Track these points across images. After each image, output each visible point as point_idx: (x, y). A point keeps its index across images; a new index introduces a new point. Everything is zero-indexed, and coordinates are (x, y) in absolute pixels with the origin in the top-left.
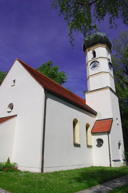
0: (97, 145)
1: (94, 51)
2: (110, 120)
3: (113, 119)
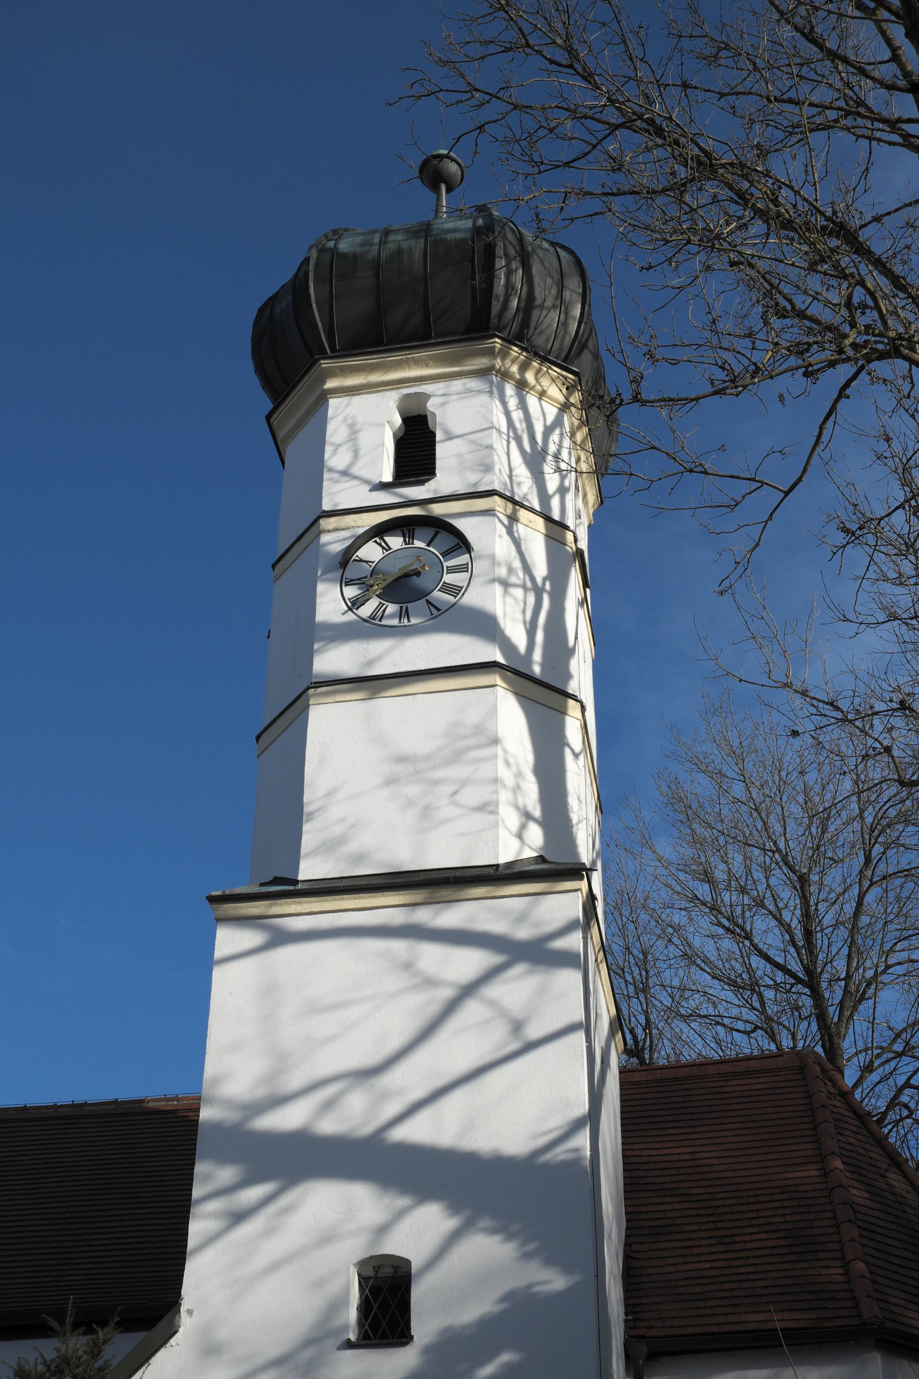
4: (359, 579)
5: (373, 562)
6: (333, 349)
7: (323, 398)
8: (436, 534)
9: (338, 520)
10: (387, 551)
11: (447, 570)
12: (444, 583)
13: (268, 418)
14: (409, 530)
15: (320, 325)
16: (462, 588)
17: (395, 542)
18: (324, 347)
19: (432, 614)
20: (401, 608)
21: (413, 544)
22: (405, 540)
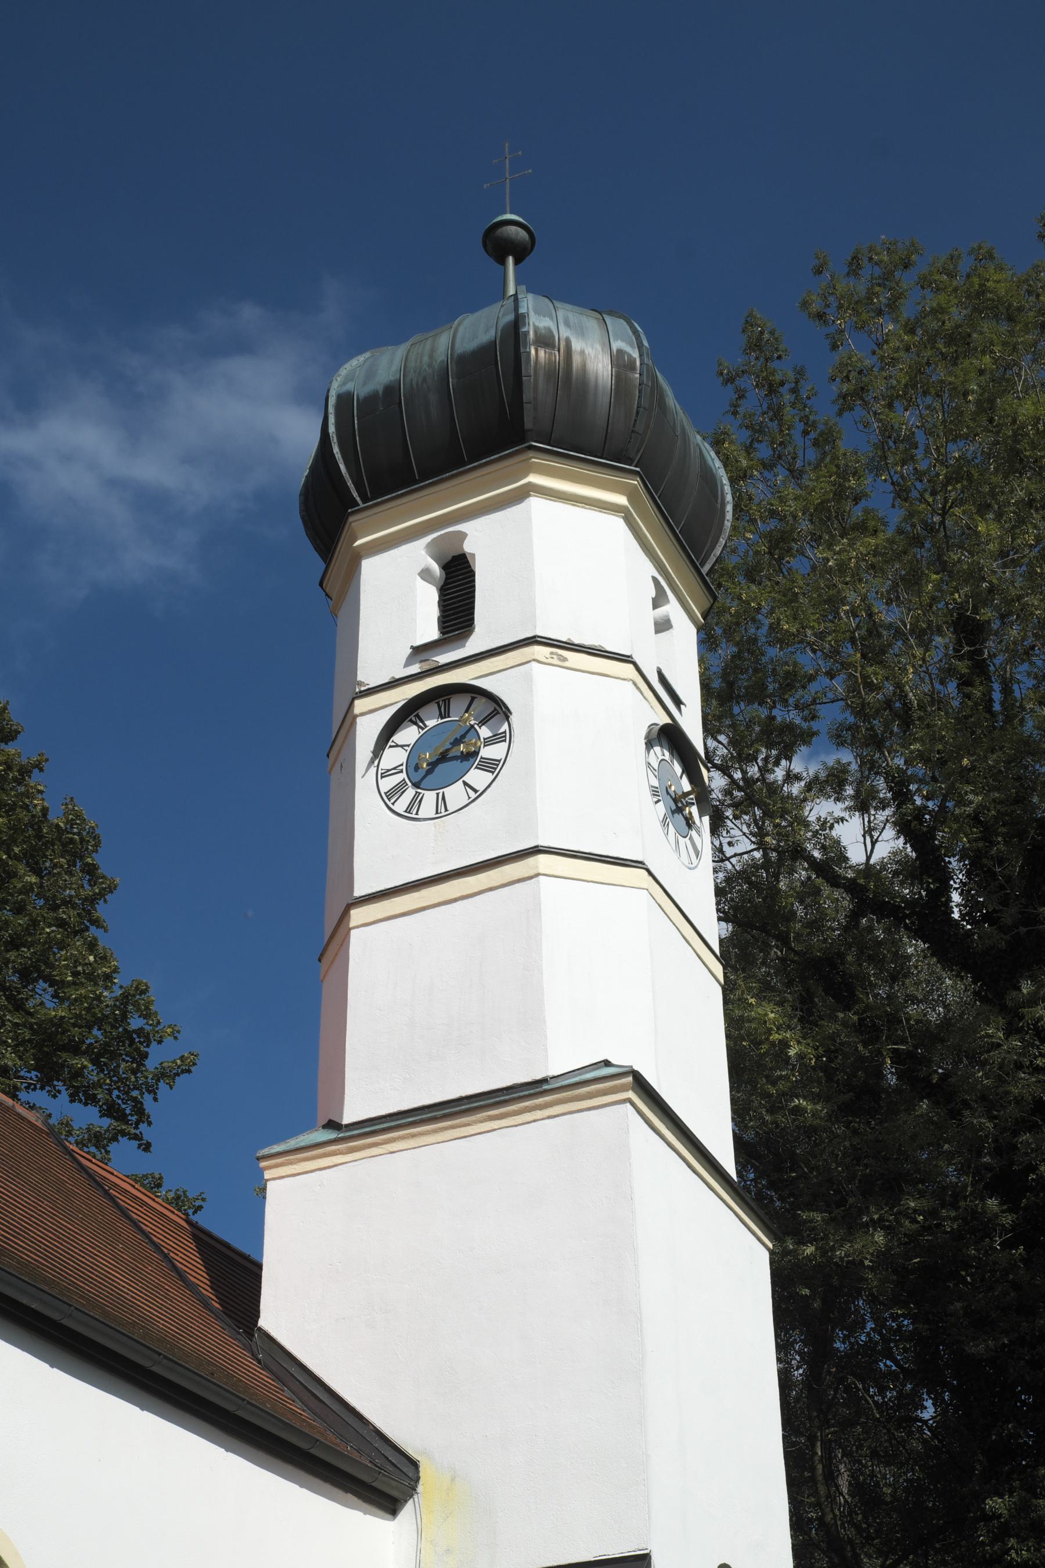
4: (394, 768)
5: (408, 746)
6: (365, 500)
10: (423, 729)
11: (405, 782)
12: (482, 758)
13: (321, 584)
14: (444, 701)
16: (499, 761)
17: (409, 735)
19: (469, 798)
20: (438, 794)
21: (426, 726)
22: (419, 727)
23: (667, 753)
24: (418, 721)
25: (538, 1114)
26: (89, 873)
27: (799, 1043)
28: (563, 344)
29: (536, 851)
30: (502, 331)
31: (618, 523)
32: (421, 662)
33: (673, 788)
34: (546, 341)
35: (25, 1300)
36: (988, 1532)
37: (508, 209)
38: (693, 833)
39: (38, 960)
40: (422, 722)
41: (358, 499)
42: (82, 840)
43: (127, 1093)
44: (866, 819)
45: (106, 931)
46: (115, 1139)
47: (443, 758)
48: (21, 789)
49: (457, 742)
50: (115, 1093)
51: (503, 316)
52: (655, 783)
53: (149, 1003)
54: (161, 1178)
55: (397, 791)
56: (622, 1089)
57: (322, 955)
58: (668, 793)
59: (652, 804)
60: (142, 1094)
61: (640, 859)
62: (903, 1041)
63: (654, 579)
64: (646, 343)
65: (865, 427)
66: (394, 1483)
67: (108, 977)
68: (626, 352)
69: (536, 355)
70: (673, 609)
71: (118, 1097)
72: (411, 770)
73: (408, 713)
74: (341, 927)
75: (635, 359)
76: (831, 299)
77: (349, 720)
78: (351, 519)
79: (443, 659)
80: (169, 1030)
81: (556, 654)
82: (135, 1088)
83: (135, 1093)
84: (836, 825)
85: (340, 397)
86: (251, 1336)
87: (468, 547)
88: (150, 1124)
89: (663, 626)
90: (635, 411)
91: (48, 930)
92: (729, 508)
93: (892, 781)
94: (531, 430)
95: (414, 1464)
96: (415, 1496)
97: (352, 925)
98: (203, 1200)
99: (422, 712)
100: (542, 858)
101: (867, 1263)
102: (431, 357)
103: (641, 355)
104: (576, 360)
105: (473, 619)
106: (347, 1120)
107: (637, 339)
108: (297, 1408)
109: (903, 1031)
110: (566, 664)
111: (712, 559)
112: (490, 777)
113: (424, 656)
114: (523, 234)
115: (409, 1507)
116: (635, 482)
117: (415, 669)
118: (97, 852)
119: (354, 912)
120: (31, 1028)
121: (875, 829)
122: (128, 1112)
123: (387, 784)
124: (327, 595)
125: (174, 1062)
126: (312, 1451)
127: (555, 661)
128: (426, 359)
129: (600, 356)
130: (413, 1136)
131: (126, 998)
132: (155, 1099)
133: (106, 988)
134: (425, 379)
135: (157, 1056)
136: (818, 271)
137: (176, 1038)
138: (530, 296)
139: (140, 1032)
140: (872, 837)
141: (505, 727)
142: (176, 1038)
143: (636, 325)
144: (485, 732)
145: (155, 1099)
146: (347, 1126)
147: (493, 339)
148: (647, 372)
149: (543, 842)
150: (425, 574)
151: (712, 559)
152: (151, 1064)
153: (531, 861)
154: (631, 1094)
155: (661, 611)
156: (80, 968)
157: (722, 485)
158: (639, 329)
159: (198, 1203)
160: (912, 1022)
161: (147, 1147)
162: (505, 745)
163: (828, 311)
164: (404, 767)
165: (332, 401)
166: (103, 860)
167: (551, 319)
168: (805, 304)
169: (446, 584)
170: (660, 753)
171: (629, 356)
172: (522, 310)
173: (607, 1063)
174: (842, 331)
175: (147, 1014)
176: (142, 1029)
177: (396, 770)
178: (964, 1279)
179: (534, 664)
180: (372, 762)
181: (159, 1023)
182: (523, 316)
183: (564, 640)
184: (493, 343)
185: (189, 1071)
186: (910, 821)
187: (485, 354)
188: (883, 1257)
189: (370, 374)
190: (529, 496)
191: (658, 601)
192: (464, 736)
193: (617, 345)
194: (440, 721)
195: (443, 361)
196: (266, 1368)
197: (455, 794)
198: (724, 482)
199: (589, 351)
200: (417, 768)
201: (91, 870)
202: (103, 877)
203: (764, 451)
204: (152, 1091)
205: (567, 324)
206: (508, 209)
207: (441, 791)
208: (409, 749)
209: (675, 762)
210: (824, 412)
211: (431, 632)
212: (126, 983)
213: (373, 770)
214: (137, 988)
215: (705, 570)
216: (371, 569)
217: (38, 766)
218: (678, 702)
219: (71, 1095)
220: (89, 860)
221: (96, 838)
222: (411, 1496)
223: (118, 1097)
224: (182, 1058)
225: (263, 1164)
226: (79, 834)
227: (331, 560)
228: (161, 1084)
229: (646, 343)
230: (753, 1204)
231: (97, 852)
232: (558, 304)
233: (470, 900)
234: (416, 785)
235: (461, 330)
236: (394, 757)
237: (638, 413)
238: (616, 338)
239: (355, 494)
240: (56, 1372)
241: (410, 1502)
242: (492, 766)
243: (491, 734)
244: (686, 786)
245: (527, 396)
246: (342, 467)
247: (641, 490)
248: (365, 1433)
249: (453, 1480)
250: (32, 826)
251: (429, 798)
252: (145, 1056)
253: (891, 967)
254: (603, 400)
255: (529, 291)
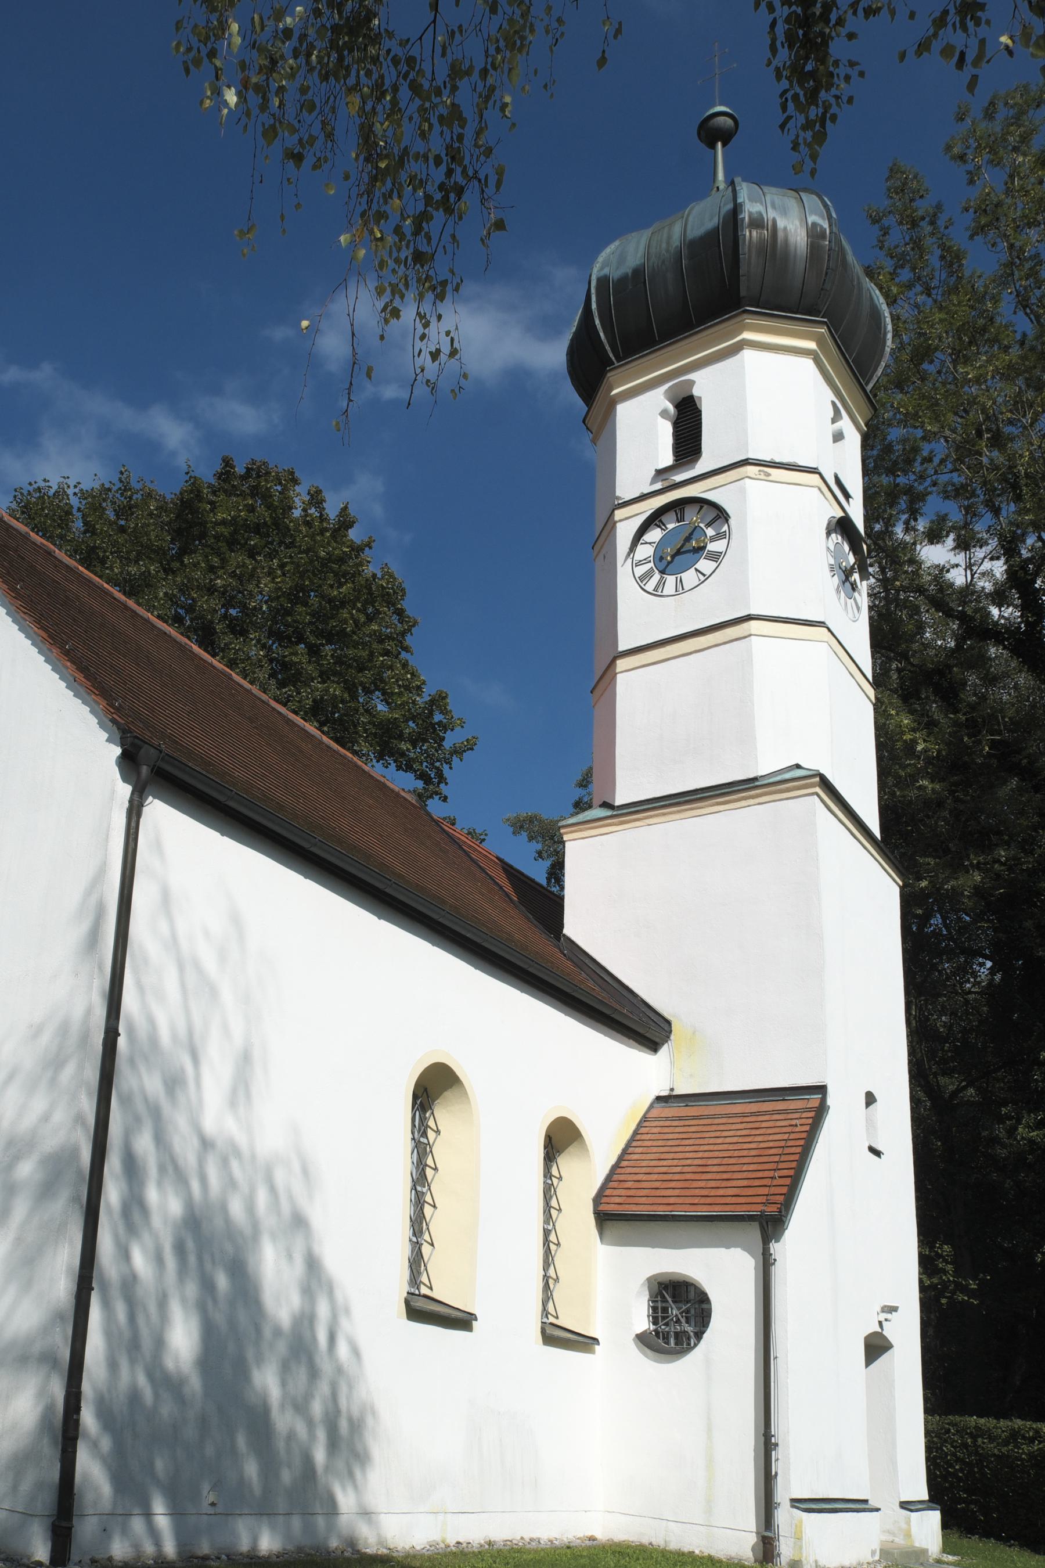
0: (642, 1339)
1: (653, 1045)
2: (794, 1103)
3: (830, 1101)
6: (619, 359)
7: (611, 405)
8: (701, 507)
9: (79, 1172)
13: (584, 422)
15: (717, 84)
17: (655, 535)
18: (611, 359)
22: (662, 529)
23: (839, 537)
24: (661, 525)
25: (751, 802)
26: (398, 615)
27: (925, 741)
28: (770, 223)
29: (749, 618)
30: (724, 217)
31: (809, 363)
32: (662, 480)
33: (844, 564)
34: (757, 223)
35: (463, 932)
36: (1041, 1073)
37: (717, 101)
38: (856, 594)
39: (375, 679)
40: (664, 525)
41: (613, 358)
42: (395, 592)
43: (432, 764)
44: (968, 556)
45: (412, 654)
46: (431, 797)
47: (678, 552)
48: (358, 561)
49: (688, 539)
50: (425, 764)
51: (724, 205)
52: (832, 562)
53: (446, 704)
54: (455, 820)
55: (647, 576)
56: (812, 785)
57: (594, 689)
58: (840, 568)
59: (830, 577)
60: (442, 764)
61: (822, 620)
62: (1000, 733)
63: (833, 403)
64: (834, 215)
65: (993, 246)
66: (657, 1034)
67: (419, 688)
68: (819, 224)
69: (750, 235)
70: (846, 424)
71: (427, 767)
72: (657, 560)
73: (654, 520)
74: (608, 673)
75: (825, 229)
76: (971, 141)
77: (610, 526)
78: (609, 375)
79: (679, 478)
80: (458, 722)
81: (763, 471)
82: (438, 761)
83: (438, 764)
84: (951, 570)
85: (599, 280)
86: (559, 940)
87: (696, 392)
88: (446, 784)
89: (838, 437)
90: (824, 273)
91: (381, 659)
92: (889, 336)
93: (1004, 541)
94: (744, 297)
95: (668, 1023)
96: (669, 1042)
97: (617, 671)
98: (486, 835)
99: (664, 518)
100: (753, 623)
101: (966, 893)
102: (668, 243)
103: (830, 226)
104: (780, 235)
105: (701, 448)
106: (618, 803)
107: (827, 212)
108: (591, 984)
109: (999, 725)
110: (770, 478)
111: (875, 379)
112: (714, 565)
113: (664, 476)
114: (729, 122)
115: (665, 1047)
116: (823, 330)
117: (658, 486)
118: (403, 600)
119: (619, 662)
120: (374, 725)
121: (974, 565)
122: (432, 776)
123: (640, 571)
124: (588, 428)
125: (462, 743)
126: (613, 1016)
127: (762, 477)
128: (664, 245)
129: (799, 230)
130: (664, 814)
131: (432, 702)
132: (451, 768)
133: (418, 695)
134: (663, 262)
135: (451, 740)
136: (961, 119)
137: (462, 727)
138: (744, 185)
139: (440, 723)
140: (972, 570)
141: (725, 528)
142: (462, 727)
143: (826, 199)
144: (710, 532)
145: (451, 768)
146: (618, 807)
147: (716, 225)
148: (835, 238)
149: (754, 611)
150: (664, 414)
151: (875, 379)
152: (447, 744)
153: (745, 625)
154: (818, 790)
155: (839, 425)
156: (400, 683)
157: (885, 317)
158: (829, 203)
159: (482, 837)
160: (1007, 720)
161: (445, 799)
162: (725, 541)
163: (968, 151)
164: (652, 558)
165: (594, 284)
166: (407, 604)
167: (761, 204)
168: (949, 148)
169: (677, 419)
170: (836, 538)
171: (821, 226)
172: (739, 200)
173: (798, 766)
174: (979, 167)
175: (444, 711)
176: (441, 722)
177: (646, 561)
178: (1035, 903)
179: (747, 480)
180: (629, 555)
181: (452, 717)
182: (741, 205)
183: (768, 460)
184: (716, 229)
185: (472, 749)
186: (1017, 571)
187: (711, 238)
188: (978, 891)
189: (622, 259)
190: (743, 349)
191: (836, 417)
192: (691, 534)
193: (812, 219)
194: (677, 524)
195: (677, 247)
196: (569, 959)
197: (689, 577)
198: (886, 315)
199: (791, 227)
200: (661, 559)
201: (400, 613)
202: (408, 617)
203: (905, 275)
204: (449, 762)
205: (774, 207)
206: (717, 101)
207: (679, 576)
208: (655, 545)
209: (845, 543)
210: (958, 238)
211: (667, 458)
212: (433, 693)
213: (629, 561)
214: (440, 696)
215: (869, 388)
216: (623, 410)
217: (369, 545)
218: (847, 496)
219: (397, 766)
220: (399, 606)
221: (403, 590)
222: (667, 1042)
223: (427, 767)
224: (467, 741)
225: (562, 831)
226: (393, 588)
227: (592, 405)
228: (454, 757)
229: (834, 215)
230: (897, 863)
231: (403, 600)
232: (766, 189)
233: (701, 653)
234: (662, 572)
235: (691, 219)
236: (644, 551)
237: (826, 273)
238: (811, 213)
239: (611, 355)
240: (478, 971)
241: (665, 1046)
242: (716, 557)
243: (714, 533)
244: (852, 559)
245: (742, 271)
246: (602, 335)
247: (827, 336)
248: (635, 1002)
249: (694, 1033)
250: (366, 587)
251: (671, 580)
252: (443, 739)
253: (1025, 705)
254: (800, 266)
255: (744, 180)
